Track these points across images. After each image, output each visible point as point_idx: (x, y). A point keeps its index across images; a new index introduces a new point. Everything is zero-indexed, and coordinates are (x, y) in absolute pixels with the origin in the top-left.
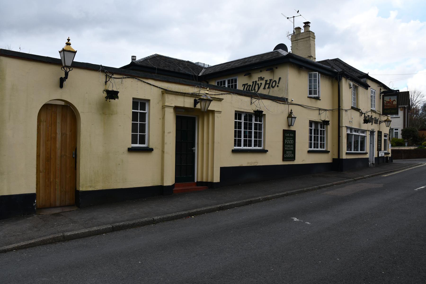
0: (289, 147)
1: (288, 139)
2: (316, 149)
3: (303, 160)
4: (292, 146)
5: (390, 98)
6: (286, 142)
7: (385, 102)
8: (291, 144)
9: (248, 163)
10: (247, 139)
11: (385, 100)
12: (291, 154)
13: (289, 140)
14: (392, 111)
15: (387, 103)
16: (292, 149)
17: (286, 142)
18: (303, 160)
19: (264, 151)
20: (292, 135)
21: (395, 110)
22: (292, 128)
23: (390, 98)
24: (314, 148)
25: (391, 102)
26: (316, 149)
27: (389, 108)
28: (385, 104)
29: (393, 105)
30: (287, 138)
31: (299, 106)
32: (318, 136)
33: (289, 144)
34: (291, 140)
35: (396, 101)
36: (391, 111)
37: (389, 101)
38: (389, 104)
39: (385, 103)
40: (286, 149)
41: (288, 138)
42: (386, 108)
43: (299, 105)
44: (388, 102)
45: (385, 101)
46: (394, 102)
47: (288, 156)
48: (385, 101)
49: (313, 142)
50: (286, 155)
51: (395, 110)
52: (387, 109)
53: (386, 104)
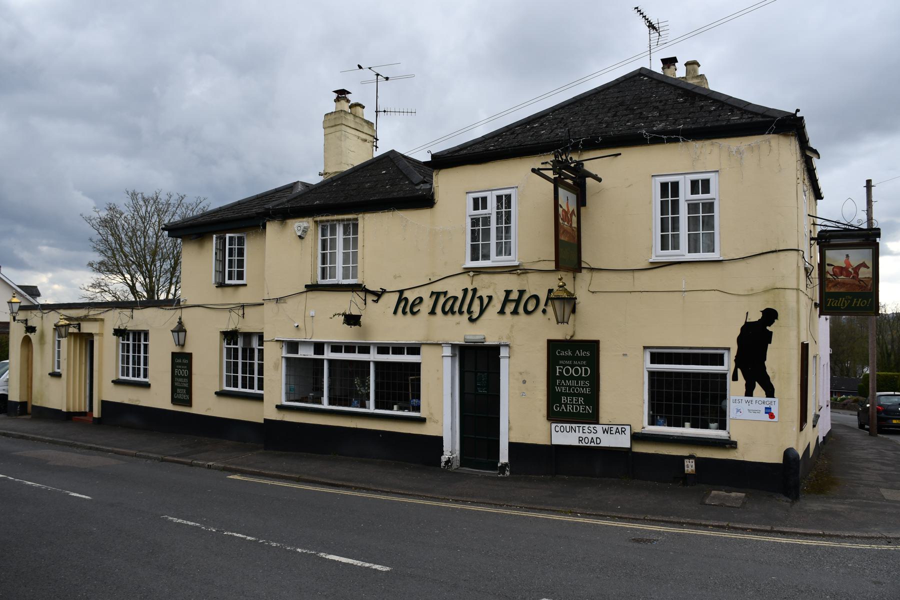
0: (570, 387)
1: (179, 368)
2: (247, 390)
3: (208, 409)
4: (186, 380)
5: (847, 256)
6: (177, 373)
7: (829, 269)
8: (184, 377)
9: (130, 400)
10: (247, 362)
11: (827, 262)
12: (582, 404)
13: (581, 366)
14: (856, 304)
15: (835, 274)
16: (186, 385)
17: (177, 373)
18: (208, 409)
19: (147, 386)
20: (186, 361)
21: (868, 301)
22: (187, 350)
23: (847, 256)
24: (244, 386)
25: (850, 270)
26: (247, 390)
27: (842, 290)
28: (831, 277)
29: (860, 280)
30: (177, 367)
31: (200, 308)
32: (140, 368)
33: (181, 377)
34: (184, 369)
35: (869, 268)
36: (852, 303)
37: (844, 265)
38: (842, 277)
39: (828, 272)
40: (558, 389)
41: (180, 367)
42: (833, 290)
43: (199, 306)
44: (841, 268)
45: (829, 265)
46: (862, 270)
47: (180, 397)
48: (829, 265)
49: (256, 376)
50: (560, 407)
51: (868, 301)
52: (837, 296)
53: (831, 275)
